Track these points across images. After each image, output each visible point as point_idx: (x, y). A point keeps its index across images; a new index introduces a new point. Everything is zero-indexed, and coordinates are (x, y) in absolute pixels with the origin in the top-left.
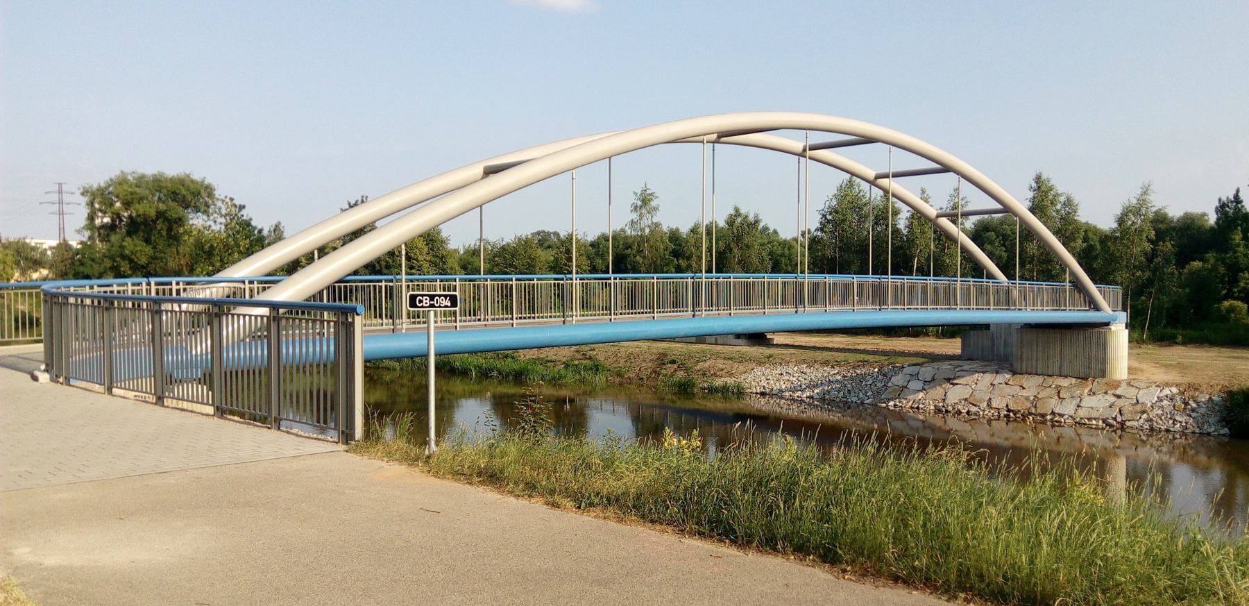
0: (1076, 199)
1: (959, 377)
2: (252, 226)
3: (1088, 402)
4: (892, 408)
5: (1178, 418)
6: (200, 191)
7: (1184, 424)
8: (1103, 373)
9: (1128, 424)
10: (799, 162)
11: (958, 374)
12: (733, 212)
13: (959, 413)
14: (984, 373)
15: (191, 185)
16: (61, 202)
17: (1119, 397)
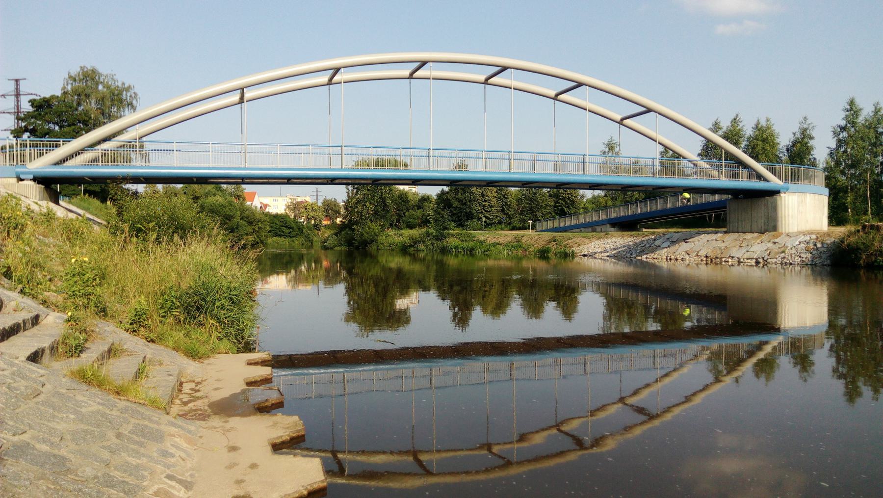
2: (36, 450)
4: (645, 260)
5: (802, 255)
6: (191, 489)
8: (775, 228)
13: (677, 260)
16: (317, 196)
17: (775, 243)
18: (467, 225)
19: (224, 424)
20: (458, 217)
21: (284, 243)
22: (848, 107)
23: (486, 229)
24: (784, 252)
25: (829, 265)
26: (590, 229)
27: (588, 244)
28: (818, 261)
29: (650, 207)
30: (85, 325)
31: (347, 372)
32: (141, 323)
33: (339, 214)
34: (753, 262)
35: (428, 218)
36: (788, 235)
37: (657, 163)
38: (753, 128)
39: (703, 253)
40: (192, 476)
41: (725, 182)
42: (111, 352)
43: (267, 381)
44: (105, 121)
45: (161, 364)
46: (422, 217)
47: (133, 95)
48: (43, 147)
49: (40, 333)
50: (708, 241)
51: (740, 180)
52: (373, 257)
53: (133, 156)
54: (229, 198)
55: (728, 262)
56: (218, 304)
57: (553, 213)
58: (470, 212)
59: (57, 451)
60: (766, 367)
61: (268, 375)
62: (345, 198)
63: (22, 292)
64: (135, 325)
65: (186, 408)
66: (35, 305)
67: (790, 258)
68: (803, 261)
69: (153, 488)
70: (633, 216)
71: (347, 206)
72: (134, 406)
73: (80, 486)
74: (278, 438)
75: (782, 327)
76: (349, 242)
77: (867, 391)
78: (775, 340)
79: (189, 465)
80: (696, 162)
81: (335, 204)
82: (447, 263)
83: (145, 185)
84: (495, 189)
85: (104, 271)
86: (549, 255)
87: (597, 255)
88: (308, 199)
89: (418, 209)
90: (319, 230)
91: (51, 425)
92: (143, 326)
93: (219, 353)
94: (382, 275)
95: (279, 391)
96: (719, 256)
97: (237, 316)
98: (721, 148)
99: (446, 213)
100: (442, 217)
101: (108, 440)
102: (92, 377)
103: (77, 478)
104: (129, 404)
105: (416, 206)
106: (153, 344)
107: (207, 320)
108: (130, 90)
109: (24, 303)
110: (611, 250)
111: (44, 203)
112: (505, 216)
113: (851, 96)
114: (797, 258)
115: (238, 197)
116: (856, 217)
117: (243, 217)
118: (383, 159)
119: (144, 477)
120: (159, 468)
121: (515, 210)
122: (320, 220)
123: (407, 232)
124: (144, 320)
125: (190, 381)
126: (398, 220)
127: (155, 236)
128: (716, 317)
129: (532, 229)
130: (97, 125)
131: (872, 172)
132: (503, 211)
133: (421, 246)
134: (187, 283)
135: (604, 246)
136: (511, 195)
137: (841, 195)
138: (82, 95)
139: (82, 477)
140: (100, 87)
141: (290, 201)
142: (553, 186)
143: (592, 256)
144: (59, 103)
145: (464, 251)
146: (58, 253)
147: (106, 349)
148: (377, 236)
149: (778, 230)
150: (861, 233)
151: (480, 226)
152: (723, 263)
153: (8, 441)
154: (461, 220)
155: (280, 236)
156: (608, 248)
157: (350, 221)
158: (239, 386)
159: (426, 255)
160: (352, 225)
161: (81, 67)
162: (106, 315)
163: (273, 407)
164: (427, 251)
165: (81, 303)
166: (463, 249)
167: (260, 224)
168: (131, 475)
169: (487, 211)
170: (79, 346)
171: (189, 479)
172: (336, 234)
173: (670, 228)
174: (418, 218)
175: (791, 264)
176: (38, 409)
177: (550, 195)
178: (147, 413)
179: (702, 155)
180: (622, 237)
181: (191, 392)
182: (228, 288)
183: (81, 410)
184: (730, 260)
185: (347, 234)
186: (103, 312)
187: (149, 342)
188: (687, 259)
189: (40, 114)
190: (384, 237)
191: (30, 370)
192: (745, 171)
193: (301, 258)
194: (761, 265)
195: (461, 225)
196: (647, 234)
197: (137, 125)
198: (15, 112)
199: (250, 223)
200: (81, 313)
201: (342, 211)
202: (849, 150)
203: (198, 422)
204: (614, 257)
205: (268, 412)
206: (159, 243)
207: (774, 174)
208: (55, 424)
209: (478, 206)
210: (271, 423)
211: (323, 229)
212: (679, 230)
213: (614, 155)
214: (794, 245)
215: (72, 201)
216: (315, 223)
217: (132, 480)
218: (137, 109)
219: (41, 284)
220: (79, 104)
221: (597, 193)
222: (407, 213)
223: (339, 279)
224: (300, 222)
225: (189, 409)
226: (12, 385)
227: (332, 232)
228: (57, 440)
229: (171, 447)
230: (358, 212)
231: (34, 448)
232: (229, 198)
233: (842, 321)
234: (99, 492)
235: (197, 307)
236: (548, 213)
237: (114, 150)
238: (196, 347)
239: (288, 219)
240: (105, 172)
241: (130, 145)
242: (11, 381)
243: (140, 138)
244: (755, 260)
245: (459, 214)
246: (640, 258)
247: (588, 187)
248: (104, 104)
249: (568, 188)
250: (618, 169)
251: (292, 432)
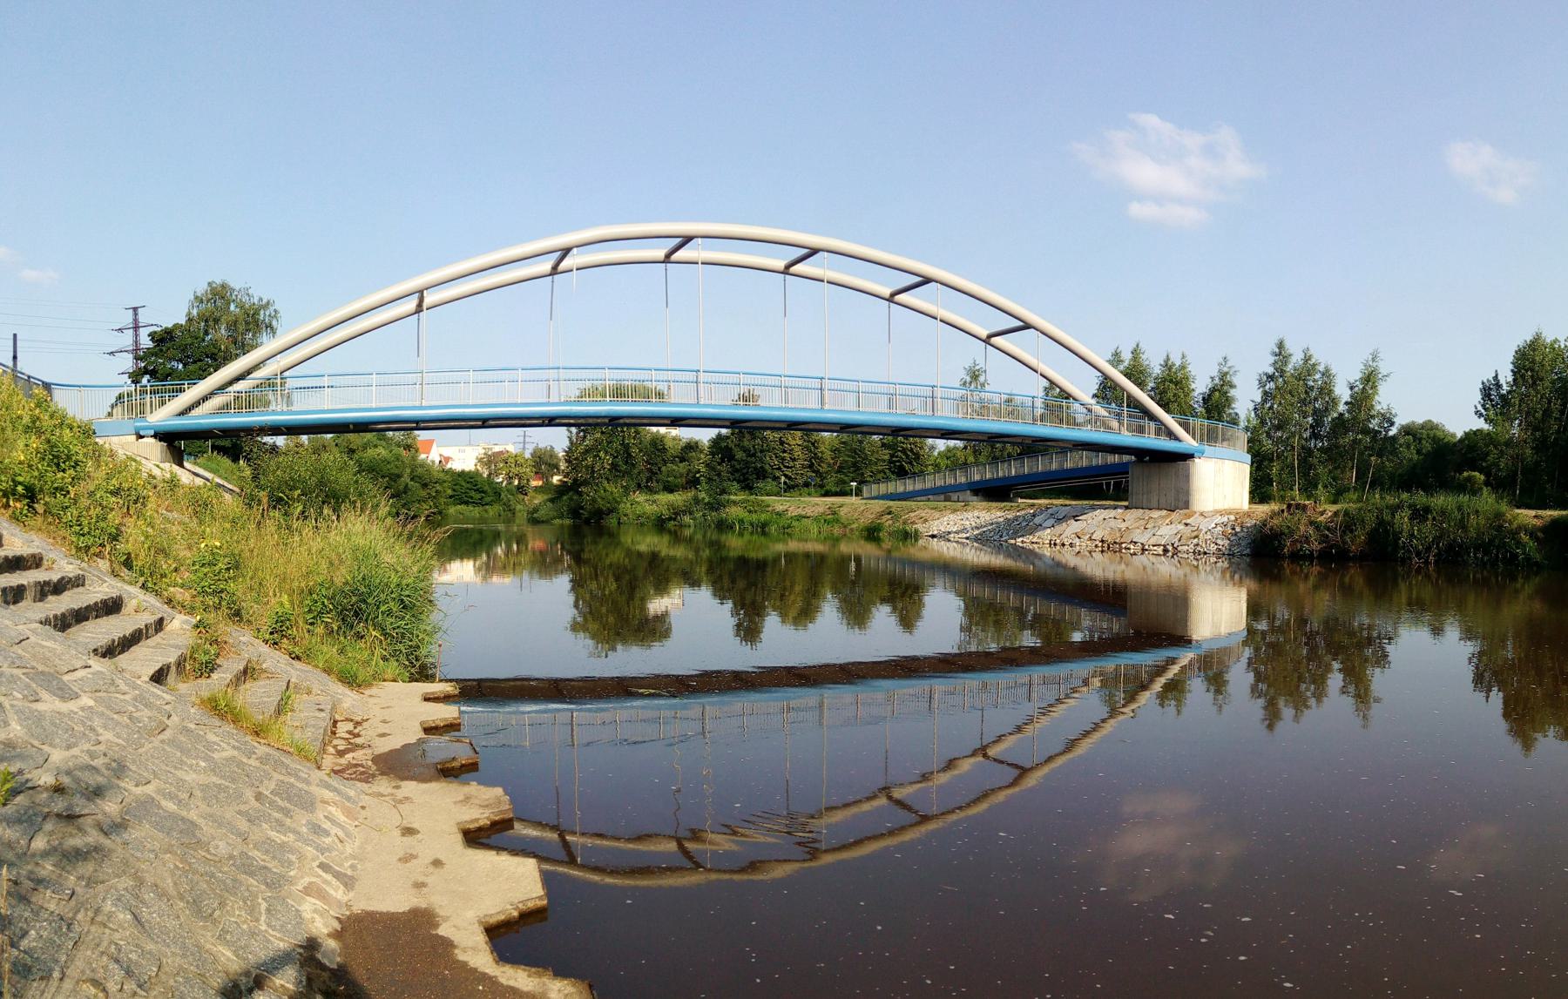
4: (1021, 545)
5: (1219, 542)
8: (1187, 505)
10: (15, 357)
13: (1063, 545)
16: (524, 443)
17: (1186, 525)
18: (757, 487)
19: (395, 791)
20: (744, 475)
22: (1277, 350)
23: (786, 494)
24: (1196, 537)
25: (1248, 555)
26: (942, 497)
27: (938, 519)
28: (1236, 550)
29: (1028, 467)
30: (215, 634)
31: (577, 710)
32: (284, 633)
33: (558, 469)
34: (1160, 550)
35: (698, 475)
36: (1202, 514)
37: (1039, 403)
38: (1161, 365)
40: (353, 867)
41: (1127, 438)
42: (247, 673)
43: (452, 727)
44: (238, 352)
45: (309, 693)
46: (688, 474)
47: (273, 314)
48: (165, 393)
49: (165, 642)
50: (1104, 519)
51: (1147, 435)
52: (613, 536)
53: (271, 396)
54: (396, 450)
55: (1129, 549)
56: (383, 608)
57: (887, 471)
58: (762, 467)
59: (185, 813)
60: (1174, 689)
61: (455, 719)
62: (566, 443)
63: (143, 586)
64: (276, 635)
65: (343, 761)
66: (158, 604)
67: (1204, 546)
68: (1220, 550)
69: (302, 881)
70: (1004, 478)
71: (570, 457)
72: (277, 754)
73: (212, 868)
74: (472, 821)
75: (1195, 637)
76: (575, 512)
77: (1287, 712)
78: (1186, 657)
79: (349, 850)
80: (1090, 406)
81: (552, 454)
82: (727, 544)
83: (285, 437)
84: (799, 433)
85: (237, 558)
87: (952, 535)
88: (512, 449)
89: (681, 462)
91: (179, 773)
92: (286, 636)
93: (384, 680)
95: (472, 745)
96: (1117, 541)
97: (409, 626)
98: (1123, 390)
99: (724, 468)
100: (719, 475)
101: (245, 803)
102: (225, 709)
103: (208, 857)
104: (271, 751)
105: (677, 457)
106: (298, 662)
107: (368, 630)
109: (145, 601)
110: (972, 529)
111: (167, 466)
112: (814, 475)
114: (1212, 545)
115: (408, 447)
116: (1282, 493)
117: (414, 476)
118: (621, 386)
119: (290, 863)
120: (310, 851)
121: (829, 465)
122: (528, 480)
123: (665, 498)
124: (288, 628)
125: (347, 720)
126: (649, 479)
127: (300, 508)
128: (1111, 625)
129: (857, 495)
130: (228, 358)
131: (1301, 437)
132: (811, 466)
133: (687, 519)
134: (341, 576)
135: (962, 522)
136: (824, 443)
137: (1266, 463)
138: (210, 320)
139: (216, 855)
140: (232, 307)
141: (484, 451)
142: (885, 431)
143: (944, 536)
144: (183, 333)
145: (753, 527)
146: (184, 532)
147: (242, 668)
148: (619, 503)
150: (1286, 514)
151: (775, 489)
152: (1124, 551)
153: (129, 794)
154: (748, 479)
155: (467, 503)
156: (968, 527)
157: (575, 480)
158: (414, 735)
159: (695, 532)
160: (580, 486)
161: (209, 283)
162: (241, 620)
163: (463, 769)
164: (695, 526)
165: (211, 603)
166: (752, 524)
167: (438, 487)
168: (274, 858)
169: (788, 467)
170: (210, 662)
171: (349, 872)
172: (552, 500)
173: (1055, 498)
174: (681, 475)
175: (1205, 553)
176: (164, 749)
177: (884, 445)
178: (293, 766)
179: (1098, 397)
180: (989, 510)
181: (348, 736)
182: (398, 585)
183: (214, 755)
184: (1132, 547)
185: (571, 499)
186: (237, 615)
187: (293, 659)
188: (1078, 544)
189: (161, 350)
190: (628, 505)
191: (154, 695)
192: (1152, 424)
193: (497, 536)
194: (1170, 554)
195: (748, 487)
196: (1023, 507)
197: (279, 356)
198: (133, 350)
199: (425, 486)
200: (211, 617)
201: (563, 466)
202: (1275, 406)
203: (359, 784)
204: (976, 539)
205: (456, 777)
206: (306, 518)
207: (1188, 432)
208: (183, 773)
209: (774, 458)
210: (461, 798)
211: (531, 493)
212: (1068, 502)
213: (979, 387)
215: (198, 461)
216: (519, 483)
217: (275, 867)
219: (166, 576)
220: (206, 333)
221: (952, 443)
222: (663, 469)
223: (560, 568)
224: (497, 483)
225: (347, 762)
226: (135, 715)
227: (546, 497)
228: (185, 796)
229: (326, 820)
230: (587, 467)
231: (159, 807)
232: (396, 450)
233: (1263, 626)
234: (235, 880)
235: (356, 611)
236: (880, 472)
237: (250, 392)
238: (354, 669)
239: (479, 479)
241: (269, 383)
242: (134, 710)
243: (281, 373)
244: (1162, 547)
245: (745, 471)
246: (1013, 541)
247: (939, 435)
248: (236, 330)
249: (911, 436)
250: (983, 409)
251: (493, 813)
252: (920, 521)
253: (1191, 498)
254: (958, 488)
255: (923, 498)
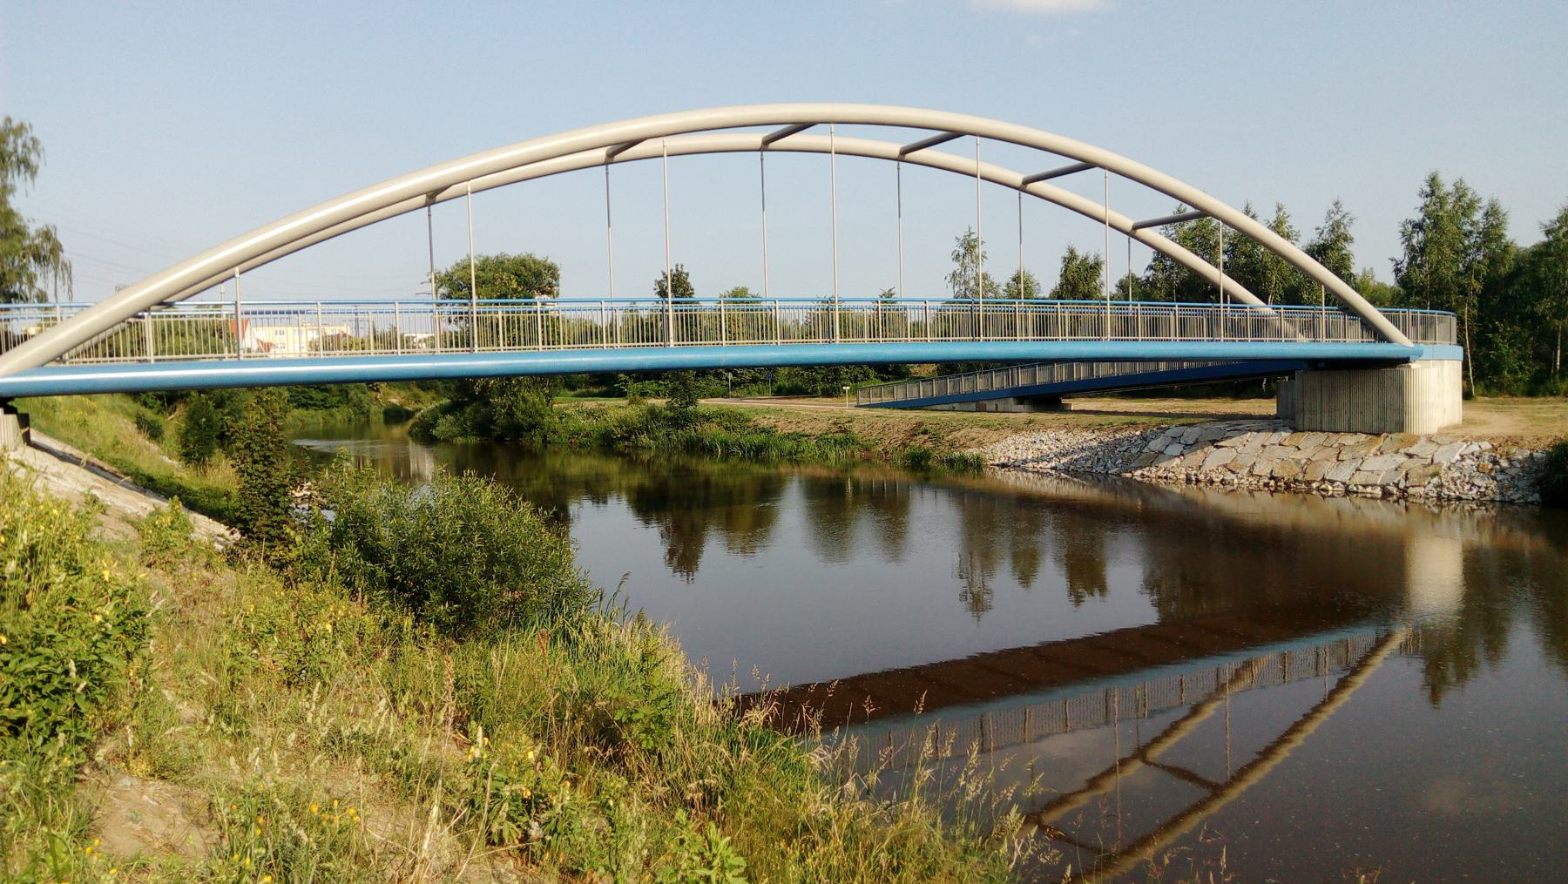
0: (1504, 207)
1: (1227, 438)
3: (1372, 463)
4: (1139, 479)
5: (1477, 482)
7: (1483, 490)
8: (1400, 427)
9: (1411, 491)
11: (1228, 434)
12: (1067, 254)
13: (1212, 482)
14: (1258, 431)
15: (532, 265)
17: (1410, 456)
21: (315, 420)
22: (1428, 189)
26: (973, 406)
34: (1378, 492)
39: (1263, 469)
47: (30, 144)
86: (930, 463)
87: (1030, 465)
90: (378, 391)
94: (550, 488)
98: (1320, 282)
108: (24, 132)
113: (1433, 171)
114: (1467, 487)
133: (644, 439)
149: (1406, 429)
155: (305, 406)
185: (477, 411)
207: (1397, 326)
214: (1453, 461)
218: (40, 172)
240: (167, 379)
246: (1129, 475)
252: (973, 443)
253: (1406, 418)
254: (1000, 395)
255: (944, 407)
